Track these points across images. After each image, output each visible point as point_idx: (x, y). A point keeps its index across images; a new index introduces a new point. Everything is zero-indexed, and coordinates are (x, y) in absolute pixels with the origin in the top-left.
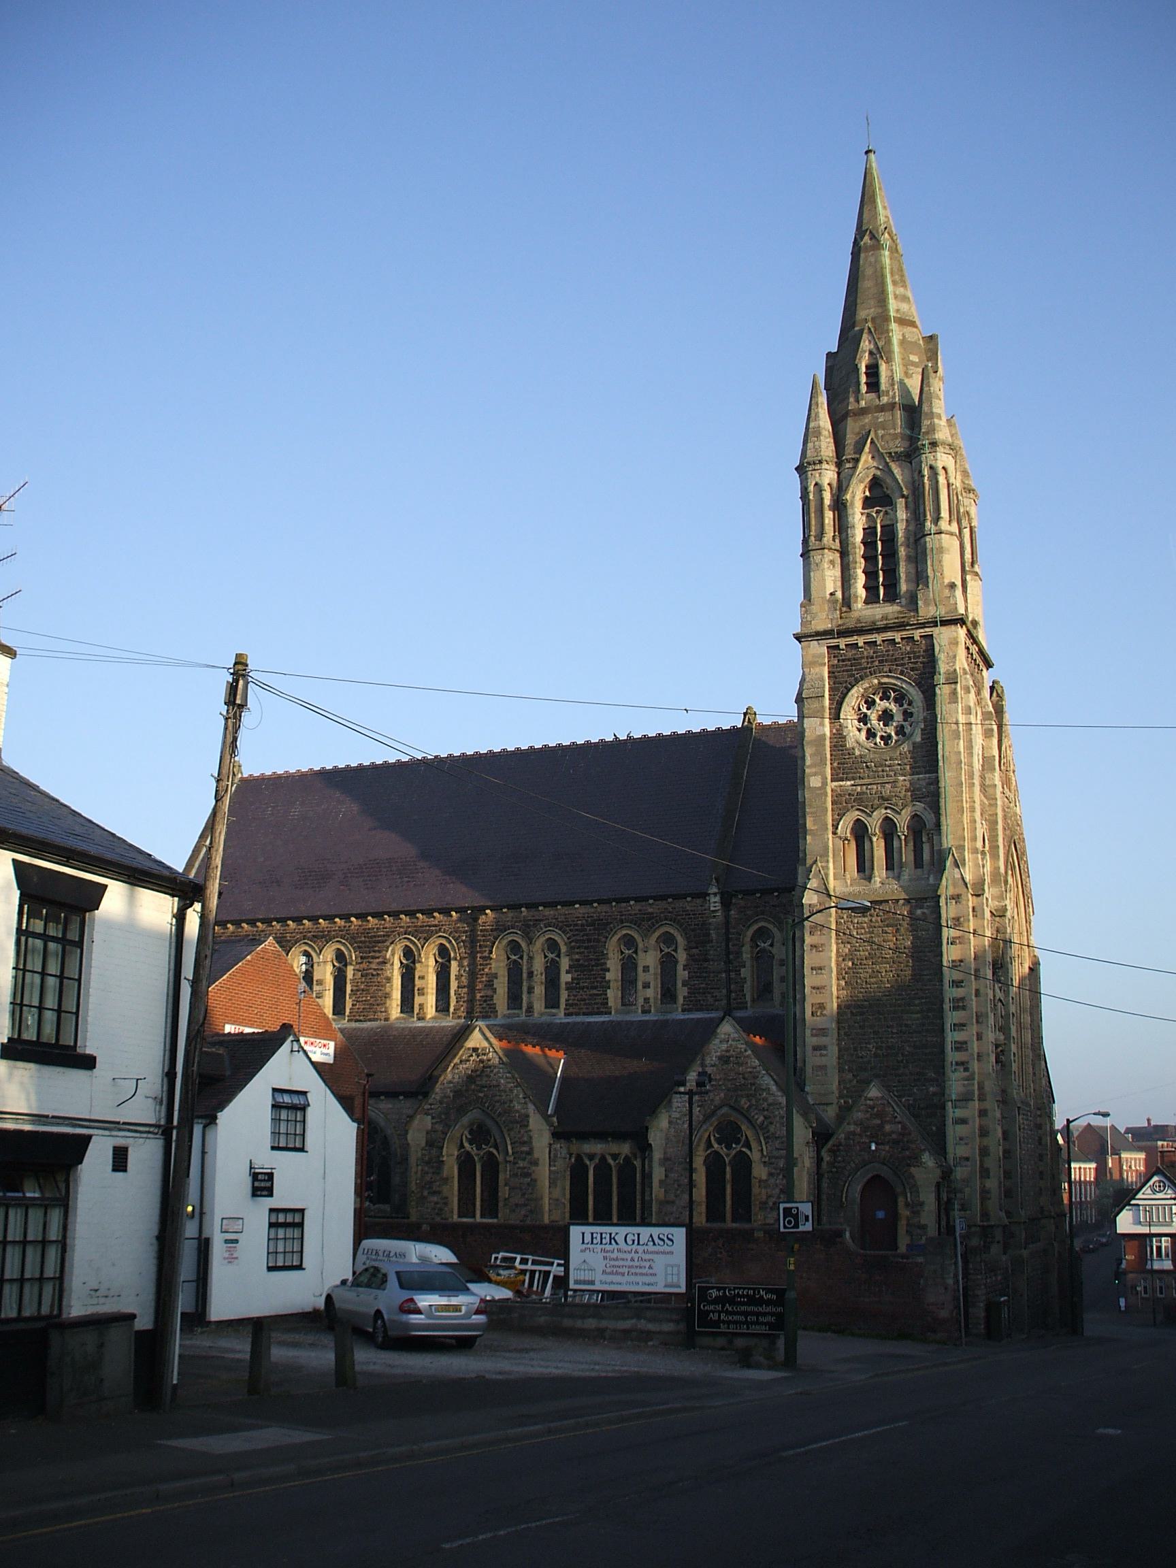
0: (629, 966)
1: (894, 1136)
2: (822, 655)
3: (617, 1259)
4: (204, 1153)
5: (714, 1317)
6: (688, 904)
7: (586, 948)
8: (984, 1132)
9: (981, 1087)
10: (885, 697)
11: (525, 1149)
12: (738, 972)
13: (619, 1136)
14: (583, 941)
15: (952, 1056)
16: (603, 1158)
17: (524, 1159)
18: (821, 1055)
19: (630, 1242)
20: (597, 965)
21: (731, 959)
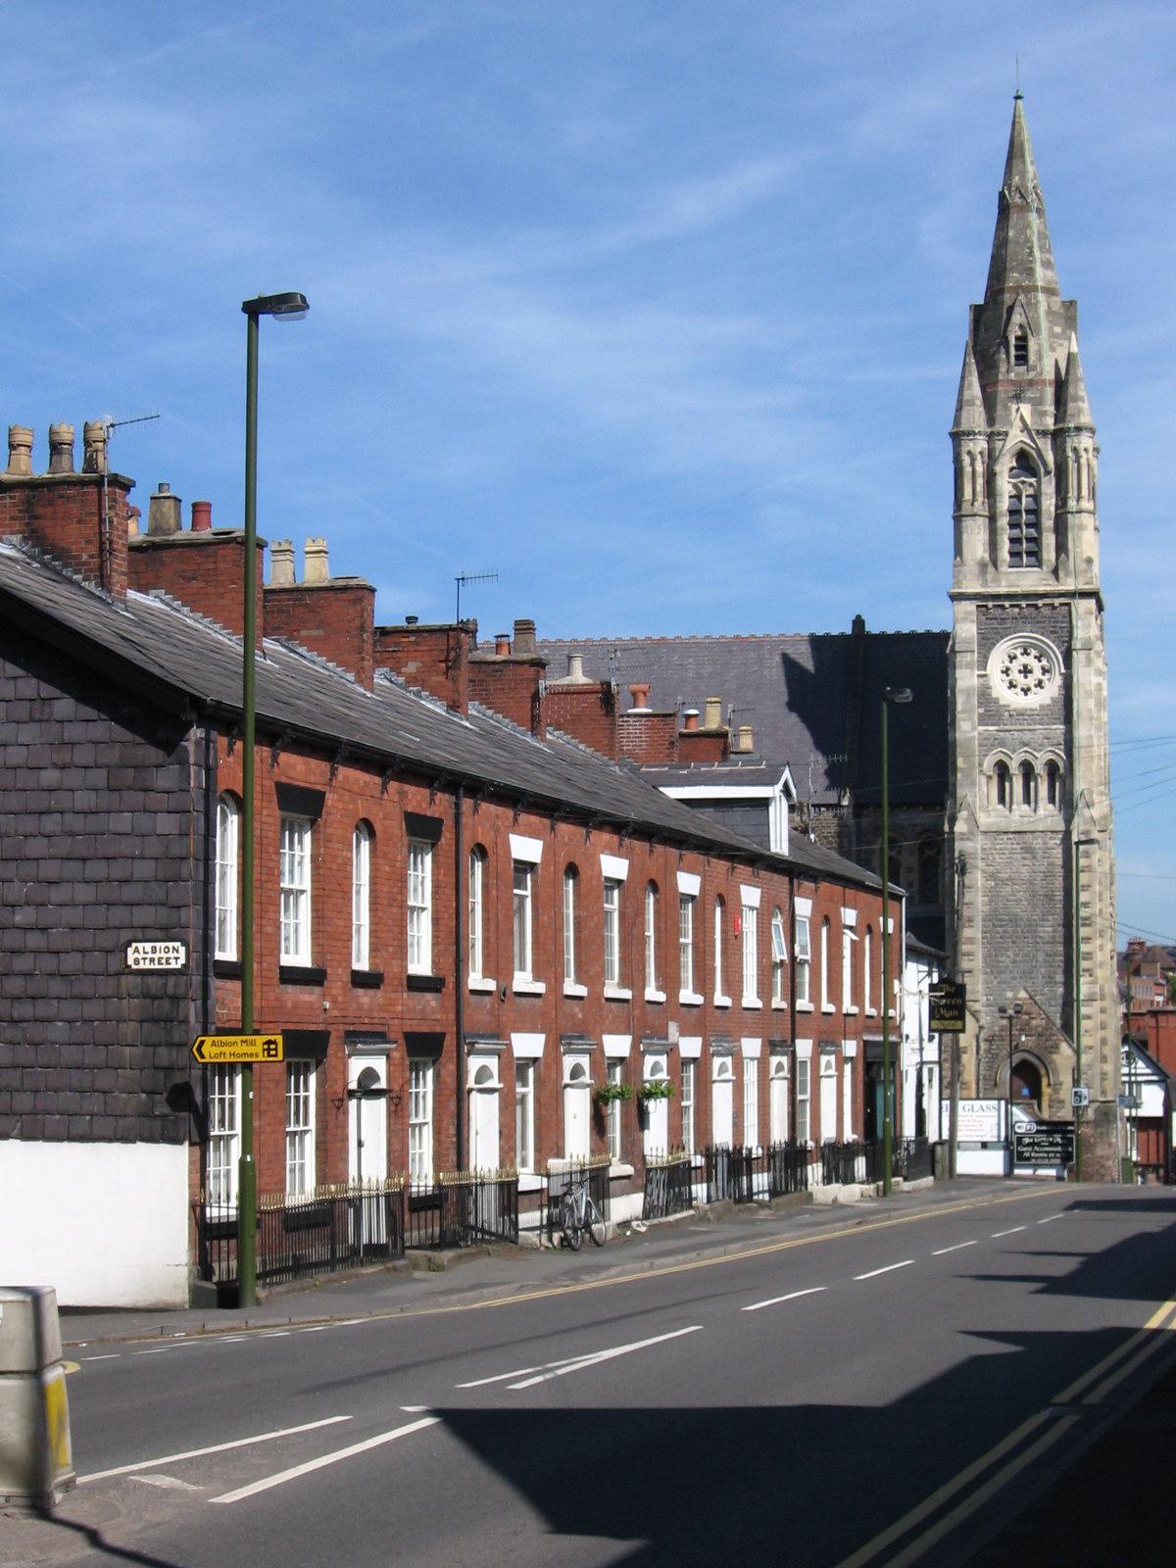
1: (1040, 1029)
2: (970, 613)
5: (1027, 1155)
10: (1026, 653)
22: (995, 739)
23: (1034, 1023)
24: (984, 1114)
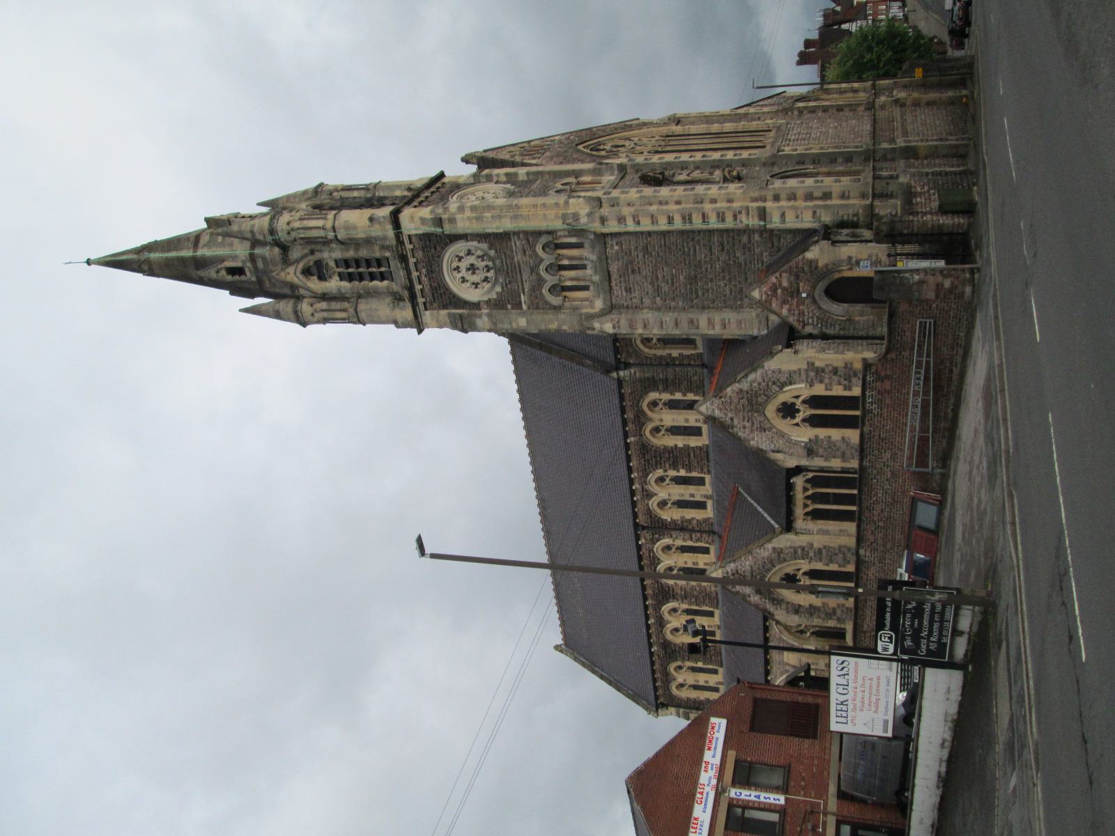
0: (675, 431)
1: (792, 278)
3: (863, 702)
4: (829, 592)
5: (933, 647)
6: (627, 390)
7: (661, 459)
8: (792, 197)
9: (754, 200)
11: (800, 551)
12: (674, 359)
13: (790, 487)
14: (656, 461)
15: (729, 223)
16: (807, 498)
17: (808, 552)
18: (729, 323)
19: (845, 691)
20: (673, 452)
21: (668, 362)
22: (531, 295)
23: (785, 284)
24: (851, 673)
